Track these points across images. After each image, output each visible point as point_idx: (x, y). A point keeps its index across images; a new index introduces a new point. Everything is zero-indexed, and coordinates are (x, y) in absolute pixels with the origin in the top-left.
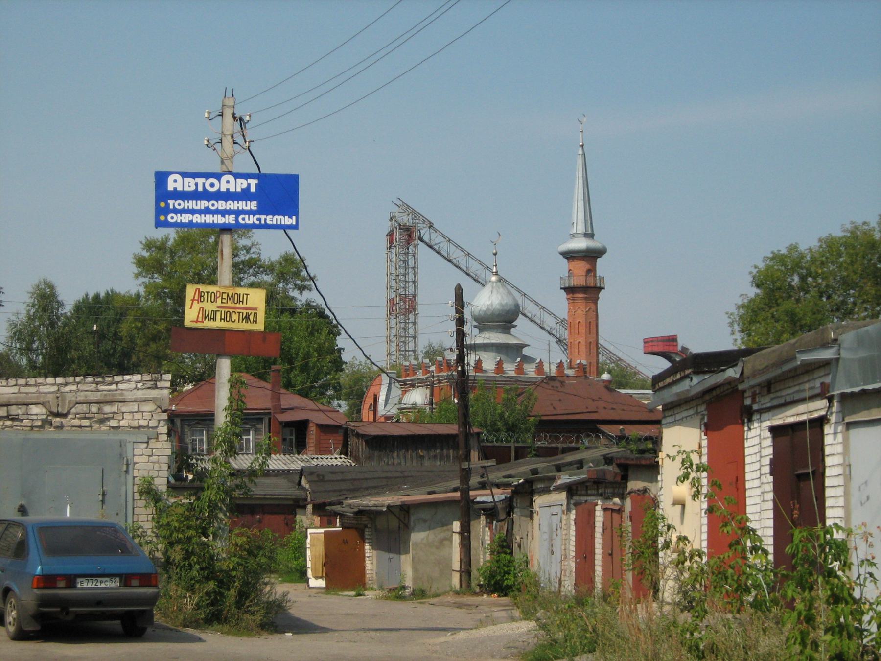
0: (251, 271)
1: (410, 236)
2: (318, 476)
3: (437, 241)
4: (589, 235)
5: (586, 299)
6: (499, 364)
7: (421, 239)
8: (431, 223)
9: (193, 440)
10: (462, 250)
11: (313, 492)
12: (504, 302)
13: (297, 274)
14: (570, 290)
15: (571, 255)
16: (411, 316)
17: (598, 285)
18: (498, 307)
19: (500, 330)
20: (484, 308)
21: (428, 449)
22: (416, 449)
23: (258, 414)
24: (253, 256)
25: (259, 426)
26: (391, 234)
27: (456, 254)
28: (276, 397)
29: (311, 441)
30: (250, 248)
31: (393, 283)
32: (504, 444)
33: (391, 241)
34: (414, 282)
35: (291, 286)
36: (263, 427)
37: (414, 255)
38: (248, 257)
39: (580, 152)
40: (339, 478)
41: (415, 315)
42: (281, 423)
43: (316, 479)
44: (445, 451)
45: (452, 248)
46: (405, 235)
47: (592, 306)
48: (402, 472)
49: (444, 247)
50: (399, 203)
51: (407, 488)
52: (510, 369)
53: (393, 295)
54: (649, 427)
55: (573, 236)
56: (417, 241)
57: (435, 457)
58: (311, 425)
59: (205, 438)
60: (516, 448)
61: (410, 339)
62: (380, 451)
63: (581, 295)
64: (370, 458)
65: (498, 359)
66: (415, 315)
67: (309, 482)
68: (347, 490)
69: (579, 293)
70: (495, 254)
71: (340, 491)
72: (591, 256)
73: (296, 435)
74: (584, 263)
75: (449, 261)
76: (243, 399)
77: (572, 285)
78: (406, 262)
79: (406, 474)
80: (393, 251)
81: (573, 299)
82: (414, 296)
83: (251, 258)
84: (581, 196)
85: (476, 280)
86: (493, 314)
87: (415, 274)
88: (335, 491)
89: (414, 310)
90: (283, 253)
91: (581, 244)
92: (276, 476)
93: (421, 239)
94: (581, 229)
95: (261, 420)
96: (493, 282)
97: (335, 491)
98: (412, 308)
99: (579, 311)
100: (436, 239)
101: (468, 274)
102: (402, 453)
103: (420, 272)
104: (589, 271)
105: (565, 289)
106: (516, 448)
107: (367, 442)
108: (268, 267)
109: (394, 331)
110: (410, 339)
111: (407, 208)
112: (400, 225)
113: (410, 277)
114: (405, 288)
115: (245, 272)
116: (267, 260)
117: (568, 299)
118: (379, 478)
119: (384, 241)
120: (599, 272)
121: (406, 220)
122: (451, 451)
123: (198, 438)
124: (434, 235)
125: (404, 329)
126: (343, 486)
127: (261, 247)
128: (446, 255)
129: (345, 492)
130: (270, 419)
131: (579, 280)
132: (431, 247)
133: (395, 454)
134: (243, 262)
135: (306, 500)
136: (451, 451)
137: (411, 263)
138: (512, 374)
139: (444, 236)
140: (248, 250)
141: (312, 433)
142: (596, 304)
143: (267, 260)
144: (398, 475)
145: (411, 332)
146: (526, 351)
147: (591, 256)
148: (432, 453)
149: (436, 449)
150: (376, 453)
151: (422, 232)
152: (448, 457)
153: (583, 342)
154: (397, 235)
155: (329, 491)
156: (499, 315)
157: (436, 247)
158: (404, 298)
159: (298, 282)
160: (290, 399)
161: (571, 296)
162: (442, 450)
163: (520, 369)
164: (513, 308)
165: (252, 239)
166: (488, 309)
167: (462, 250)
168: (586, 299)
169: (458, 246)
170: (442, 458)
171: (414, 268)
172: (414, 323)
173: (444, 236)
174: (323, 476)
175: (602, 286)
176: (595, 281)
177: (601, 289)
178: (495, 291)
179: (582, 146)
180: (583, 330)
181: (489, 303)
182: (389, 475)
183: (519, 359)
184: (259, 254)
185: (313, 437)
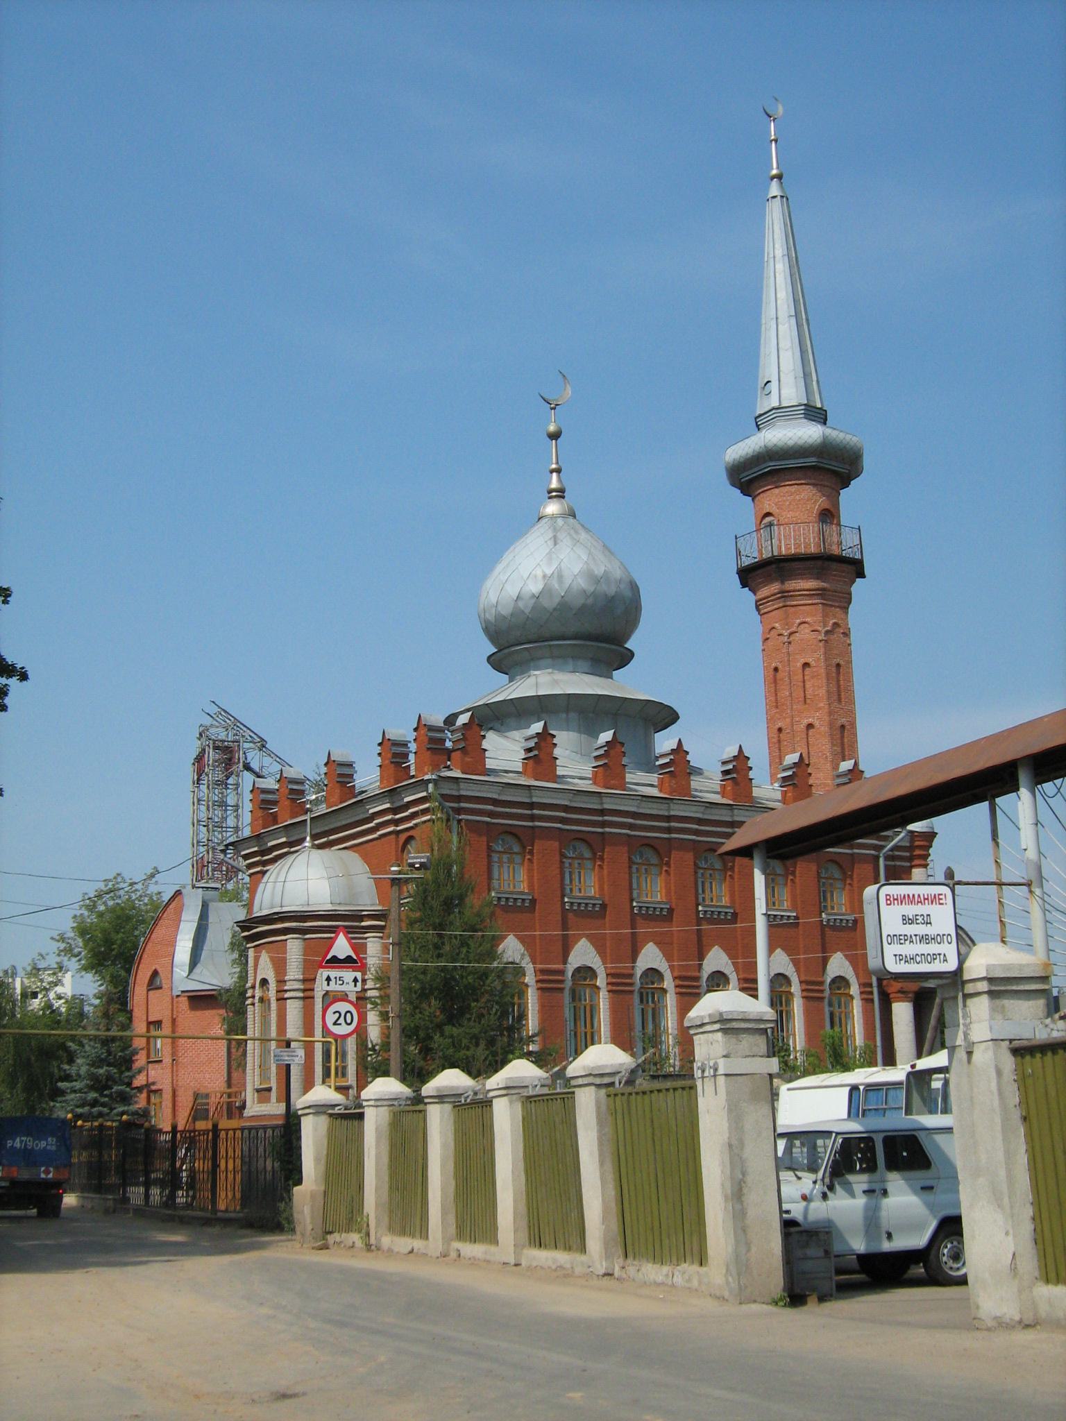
4: (815, 414)
5: (822, 593)
12: (599, 570)
18: (582, 583)
19: (584, 665)
20: (535, 587)
26: (199, 759)
33: (200, 772)
54: (170, 1105)
69: (802, 576)
70: (555, 436)
72: (832, 468)
76: (153, 1088)
86: (563, 606)
87: (237, 817)
93: (247, 767)
94: (791, 393)
99: (805, 632)
119: (189, 772)
124: (267, 761)
147: (832, 468)
151: (250, 755)
153: (822, 726)
154: (211, 755)
166: (546, 591)
178: (565, 542)
181: (549, 572)
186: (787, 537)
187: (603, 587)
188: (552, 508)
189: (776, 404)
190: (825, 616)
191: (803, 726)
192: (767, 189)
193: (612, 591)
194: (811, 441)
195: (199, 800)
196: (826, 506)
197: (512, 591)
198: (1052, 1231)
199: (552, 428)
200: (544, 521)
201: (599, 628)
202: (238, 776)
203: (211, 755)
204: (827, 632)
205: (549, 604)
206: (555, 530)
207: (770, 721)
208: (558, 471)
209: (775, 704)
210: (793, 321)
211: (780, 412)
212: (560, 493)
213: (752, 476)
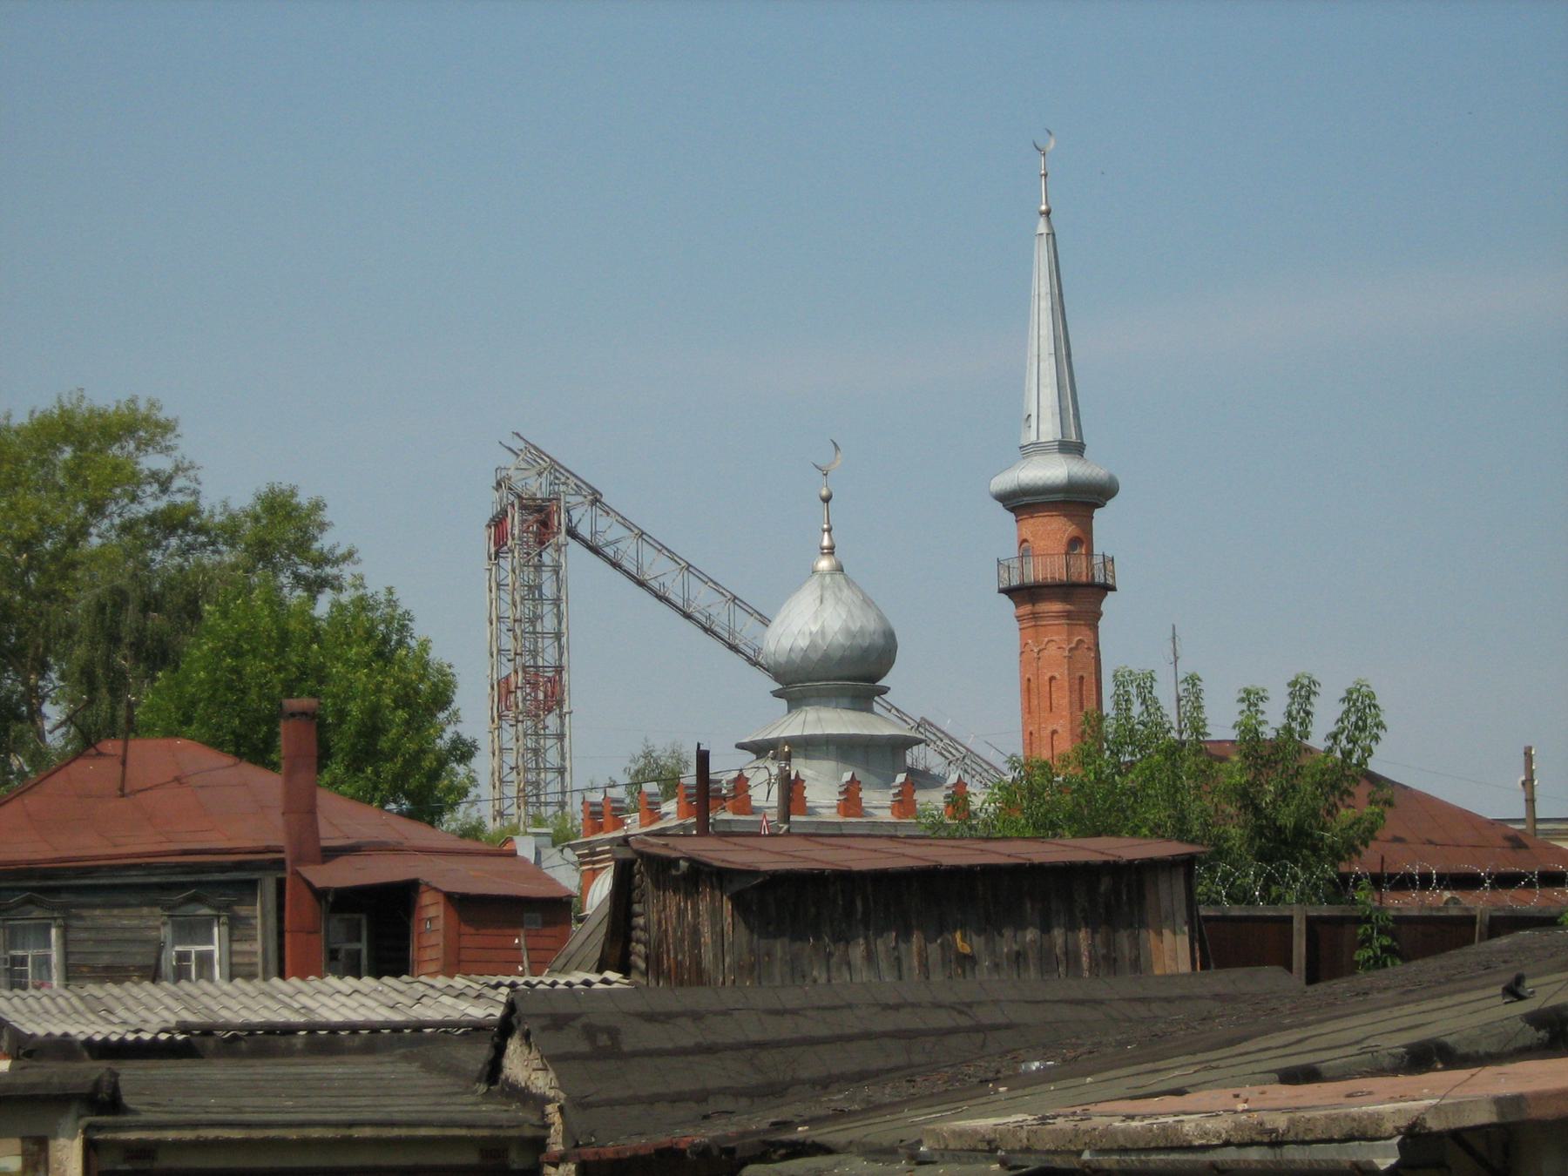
0: (174, 542)
1: (545, 524)
2: (590, 1032)
3: (610, 536)
4: (1072, 447)
5: (1068, 615)
6: (850, 794)
7: (572, 533)
8: (595, 492)
9: (15, 961)
10: (673, 556)
11: (577, 1105)
12: (855, 627)
13: (301, 546)
14: (1022, 593)
15: (1027, 500)
16: (552, 721)
17: (1100, 578)
18: (841, 639)
19: (845, 701)
20: (803, 643)
21: (990, 924)
22: (943, 927)
23: (239, 866)
24: (179, 498)
25: (243, 911)
26: (498, 522)
27: (656, 567)
28: (303, 812)
29: (429, 954)
30: (170, 478)
31: (508, 642)
32: (1262, 909)
33: (500, 541)
34: (558, 636)
35: (285, 579)
36: (259, 912)
37: (556, 570)
38: (162, 503)
39: (1042, 228)
40: (688, 1042)
41: (561, 717)
42: (320, 894)
43: (584, 1047)
44: (1058, 934)
45: (648, 553)
46: (534, 522)
47: (1084, 634)
48: (962, 1008)
49: (628, 550)
50: (518, 445)
51: (1044, 1077)
52: (878, 802)
53: (507, 669)
55: (1036, 448)
56: (562, 537)
57: (1019, 958)
58: (426, 898)
59: (55, 955)
60: (1311, 922)
61: (551, 776)
62: (797, 936)
63: (1056, 607)
64: (752, 968)
65: (847, 776)
66: (561, 717)
67: (552, 1060)
68: (737, 1093)
69: (1050, 599)
70: (827, 500)
71: (702, 1096)
72: (1080, 502)
73: (377, 927)
74: (1063, 520)
75: (641, 584)
77: (1030, 578)
78: (534, 589)
79: (985, 1016)
80: (506, 564)
81: (1035, 616)
82: (559, 669)
83: (174, 507)
84: (1047, 346)
85: (707, 630)
86: (826, 657)
88: (677, 1098)
89: (560, 703)
90: (264, 489)
91: (1052, 471)
92: (368, 1048)
93: (572, 533)
94: (1049, 430)
95: (252, 885)
96: (823, 574)
97: (677, 1098)
98: (554, 700)
99: (1052, 648)
100: (608, 530)
101: (688, 616)
102: (885, 943)
103: (574, 609)
104: (1074, 543)
105: (1009, 592)
106: (1311, 922)
107: (739, 902)
108: (223, 527)
109: (510, 759)
110: (551, 776)
111: (534, 454)
112: (519, 497)
113: (549, 624)
114: (534, 654)
115: (157, 546)
116: (218, 510)
117: (1019, 618)
118: (867, 1036)
119: (482, 540)
120: (1103, 542)
121: (537, 487)
122: (1083, 935)
123: (30, 953)
124: (603, 522)
125: (536, 751)
126: (712, 1073)
127: (201, 475)
128: (633, 570)
129: (727, 1104)
130: (281, 885)
131: (1048, 567)
132: (596, 550)
133: (857, 952)
134: (152, 520)
135: (539, 1144)
136: (1083, 935)
137: (549, 590)
138: (886, 816)
139: (626, 523)
140: (165, 487)
141: (432, 915)
142: (1095, 629)
143: (218, 510)
144: (943, 1020)
145: (552, 758)
146: (918, 757)
148: (1007, 944)
149: (1021, 926)
150: (780, 947)
152: (1072, 957)
154: (515, 520)
155: (653, 1100)
156: (842, 661)
157: (609, 551)
158: (533, 676)
159: (304, 569)
160: (344, 816)
161: (1027, 609)
162: (1046, 929)
163: (904, 803)
164: (880, 641)
165: (177, 454)
166: (813, 645)
167: (673, 556)
168: (1068, 615)
169: (662, 548)
170: (1047, 961)
171: (557, 602)
172: (561, 737)
173: (626, 523)
174: (613, 1033)
175: (1110, 581)
176: (1090, 567)
177: (1108, 588)
179: (1048, 213)
180: (1062, 699)
181: (814, 629)
182: (906, 1020)
183: (901, 778)
184: (196, 493)
185: (437, 939)
186: (1045, 566)
187: (859, 641)
188: (824, 564)
189: (1033, 438)
190: (1070, 634)
191: (1048, 731)
192: (1035, 226)
193: (866, 643)
194: (1058, 481)
195: (499, 585)
196: (1076, 533)
197: (786, 643)
198: (124, 929)
199: (824, 492)
200: (816, 577)
201: (858, 673)
202: (558, 550)
203: (515, 520)
204: (1071, 650)
205: (815, 656)
206: (823, 587)
207: (1025, 724)
208: (829, 530)
209: (1028, 710)
210: (1053, 359)
211: (1036, 448)
212: (831, 550)
213: (1021, 502)
